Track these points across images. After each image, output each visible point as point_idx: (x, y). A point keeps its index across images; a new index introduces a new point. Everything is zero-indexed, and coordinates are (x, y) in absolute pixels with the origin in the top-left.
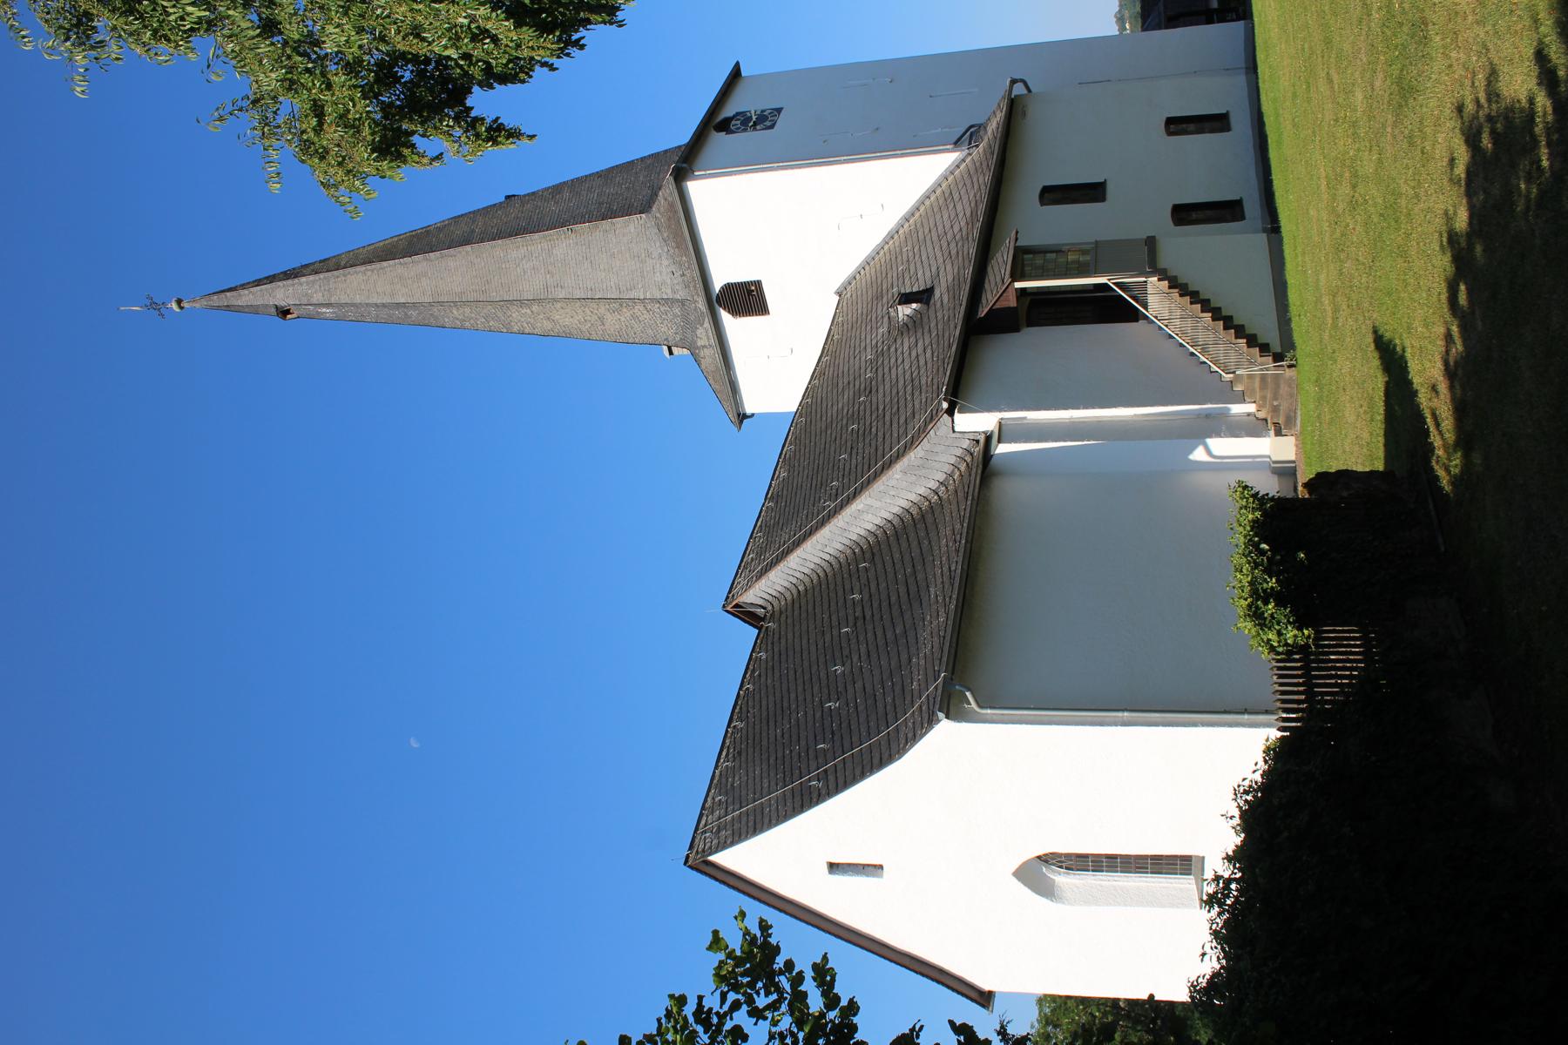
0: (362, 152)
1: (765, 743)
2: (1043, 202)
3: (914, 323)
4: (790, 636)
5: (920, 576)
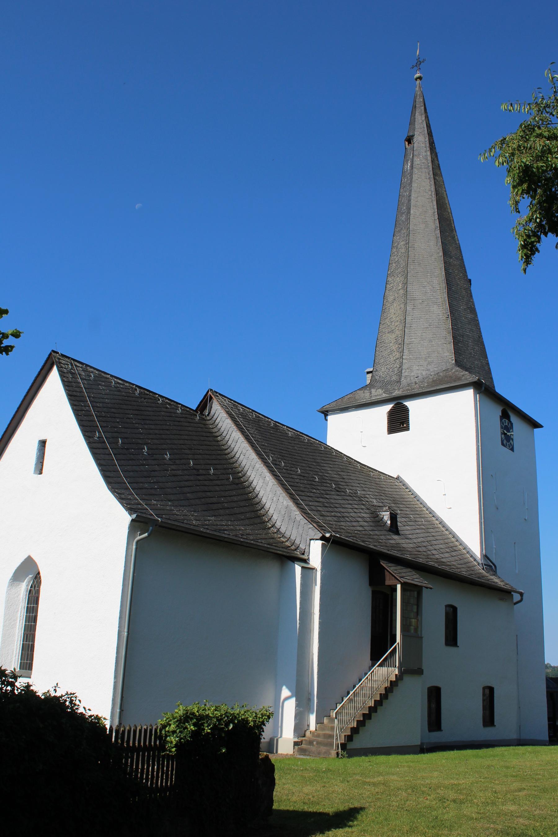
0: (526, 159)
1: (125, 407)
2: (447, 606)
3: (377, 521)
4: (190, 429)
5: (222, 512)
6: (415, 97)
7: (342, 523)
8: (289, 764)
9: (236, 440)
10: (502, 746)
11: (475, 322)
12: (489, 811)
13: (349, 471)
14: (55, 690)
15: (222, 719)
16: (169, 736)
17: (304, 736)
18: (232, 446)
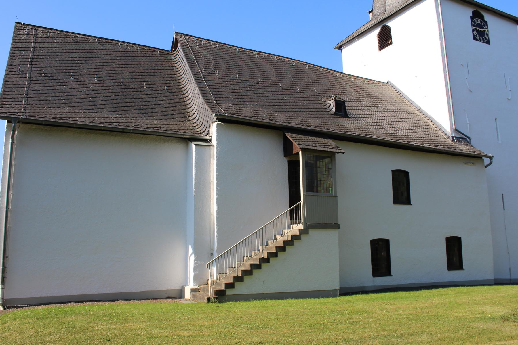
2: (394, 172)
10: (468, 286)
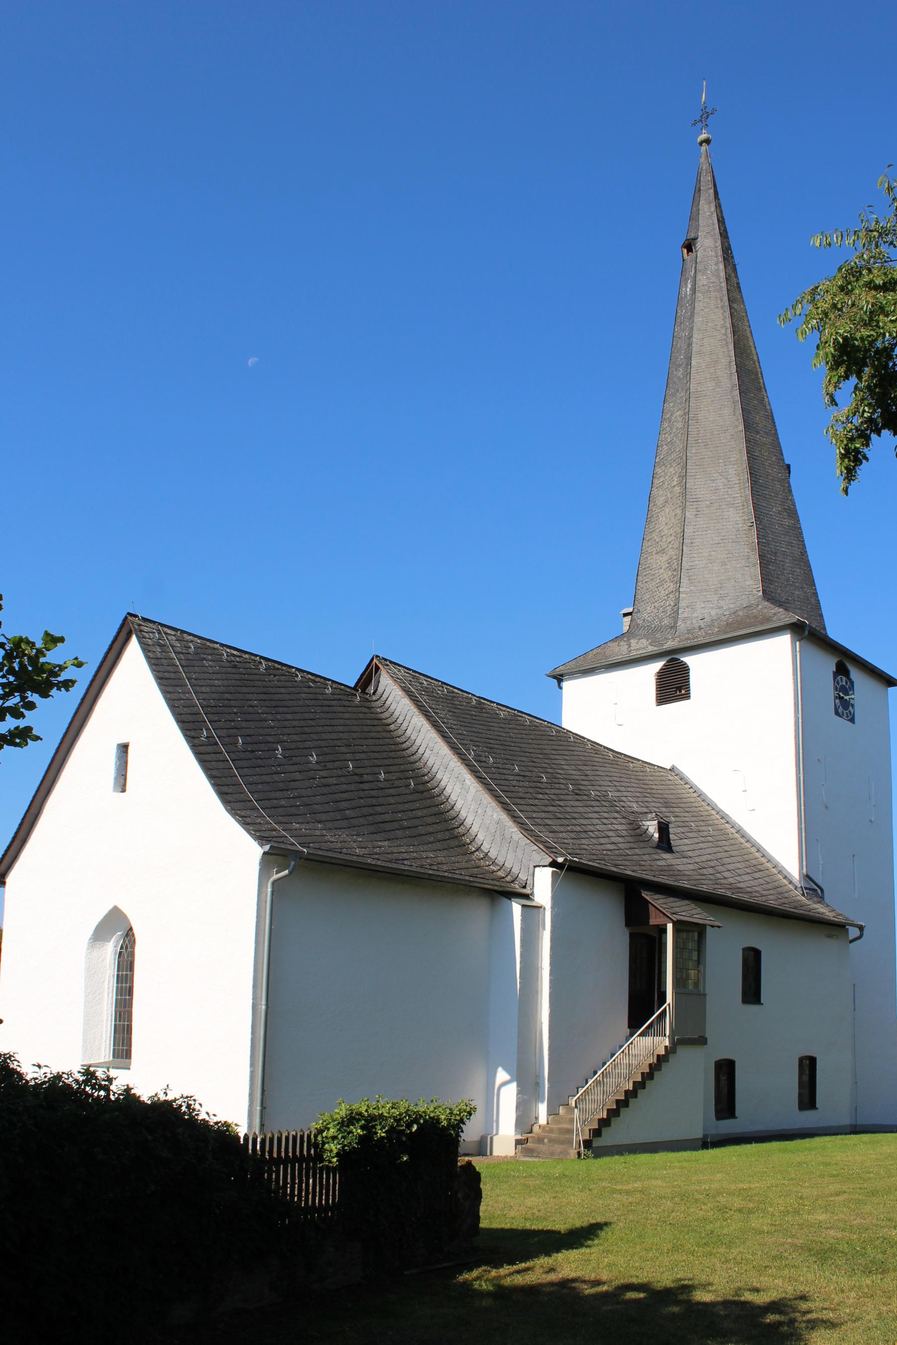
0: (844, 328)
1: (244, 690)
2: (745, 950)
3: (639, 835)
4: (346, 716)
5: (399, 833)
6: (699, 174)
7: (583, 841)
8: (507, 1170)
9: (417, 728)
10: (826, 1135)
11: (796, 531)
12: (788, 1221)
13: (595, 764)
14: (166, 1094)
15: (400, 1119)
16: (328, 1143)
17: (531, 1132)
18: (413, 738)
